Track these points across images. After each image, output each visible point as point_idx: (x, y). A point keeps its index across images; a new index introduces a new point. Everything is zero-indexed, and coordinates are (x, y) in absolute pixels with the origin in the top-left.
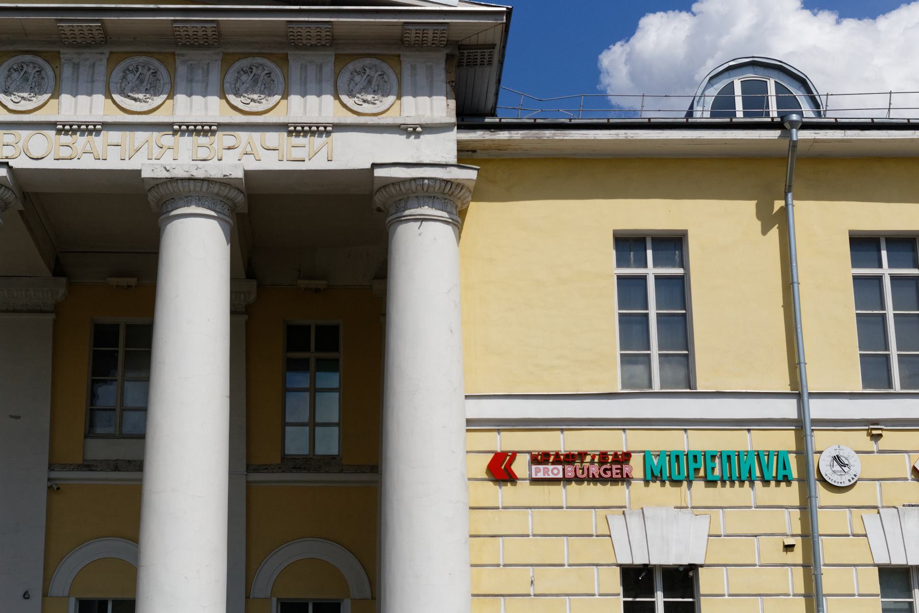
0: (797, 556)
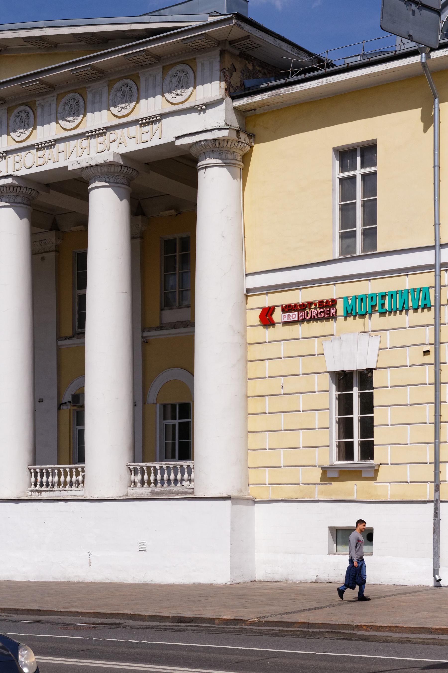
0: (431, 358)
